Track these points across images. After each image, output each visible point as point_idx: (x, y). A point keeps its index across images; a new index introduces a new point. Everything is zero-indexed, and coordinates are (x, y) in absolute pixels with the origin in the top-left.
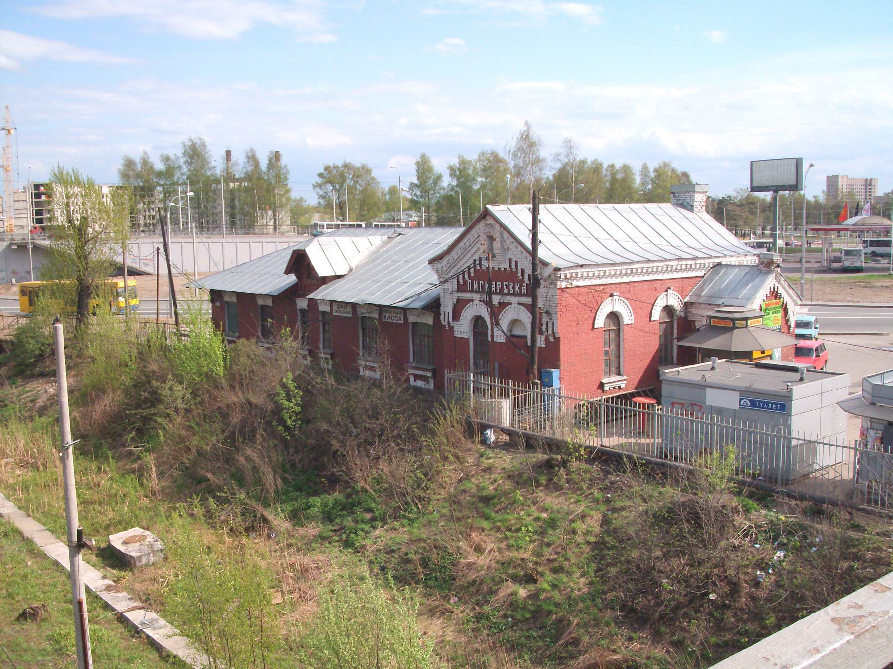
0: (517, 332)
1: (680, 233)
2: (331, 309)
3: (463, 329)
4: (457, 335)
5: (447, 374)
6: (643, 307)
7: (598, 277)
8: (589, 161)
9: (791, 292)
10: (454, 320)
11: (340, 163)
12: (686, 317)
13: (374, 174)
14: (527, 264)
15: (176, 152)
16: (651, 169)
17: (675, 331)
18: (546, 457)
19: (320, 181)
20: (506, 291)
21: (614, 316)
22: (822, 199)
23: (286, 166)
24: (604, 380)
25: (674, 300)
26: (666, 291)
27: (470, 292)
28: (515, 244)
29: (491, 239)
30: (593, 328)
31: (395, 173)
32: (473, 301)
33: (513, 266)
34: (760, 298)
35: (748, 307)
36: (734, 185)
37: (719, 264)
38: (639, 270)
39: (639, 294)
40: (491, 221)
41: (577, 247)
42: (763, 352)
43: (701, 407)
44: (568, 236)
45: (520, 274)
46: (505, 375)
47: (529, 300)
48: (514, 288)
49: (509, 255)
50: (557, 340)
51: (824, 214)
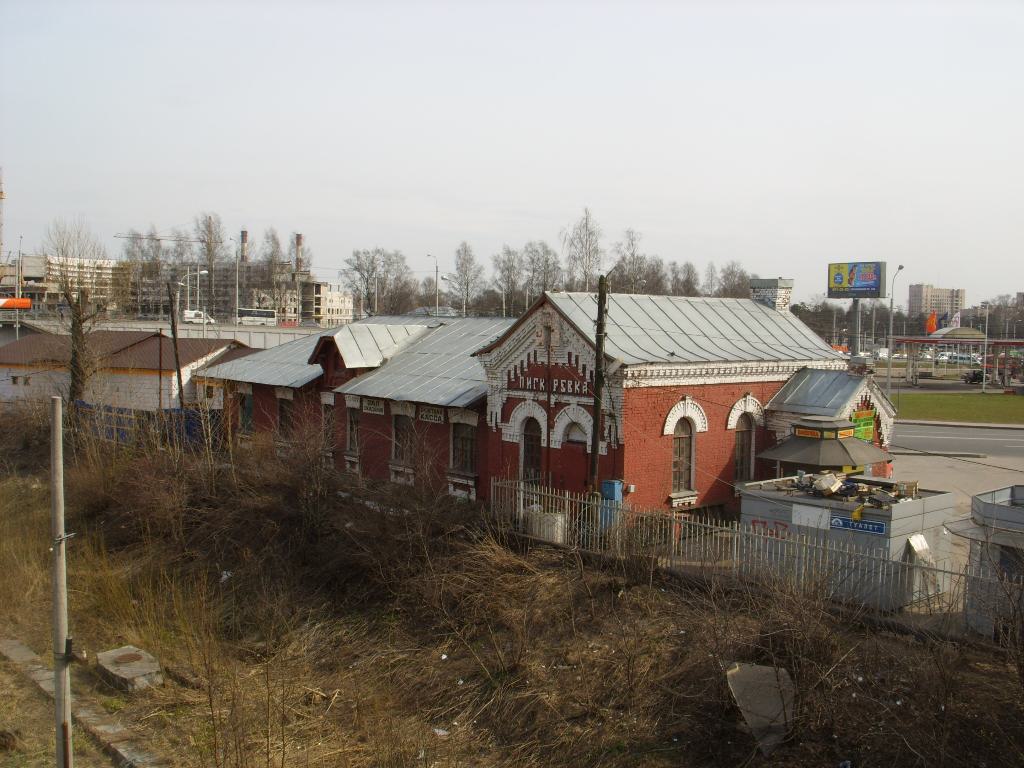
0: (576, 436)
1: (762, 333)
2: (361, 406)
3: (513, 432)
4: (506, 438)
5: (494, 483)
6: (717, 415)
7: (670, 377)
8: (647, 258)
9: (884, 401)
10: (503, 420)
11: (371, 248)
12: (765, 427)
13: (408, 262)
14: (589, 359)
15: (190, 229)
16: (718, 269)
17: (753, 441)
18: (608, 579)
19: (346, 267)
20: (563, 390)
21: (686, 423)
22: (905, 311)
23: (309, 250)
24: (673, 495)
25: (752, 406)
26: (745, 396)
27: (521, 389)
28: (577, 336)
29: (549, 329)
30: (662, 434)
31: (427, 264)
32: (525, 400)
33: (573, 362)
34: (849, 409)
35: (837, 417)
36: (811, 289)
37: (805, 368)
38: (716, 371)
39: (716, 399)
40: (549, 309)
41: (646, 343)
42: (854, 468)
43: (786, 526)
44: (635, 332)
45: (580, 371)
46: (560, 485)
47: (590, 401)
48: (573, 386)
49: (569, 349)
50: (621, 447)
51: (907, 327)
